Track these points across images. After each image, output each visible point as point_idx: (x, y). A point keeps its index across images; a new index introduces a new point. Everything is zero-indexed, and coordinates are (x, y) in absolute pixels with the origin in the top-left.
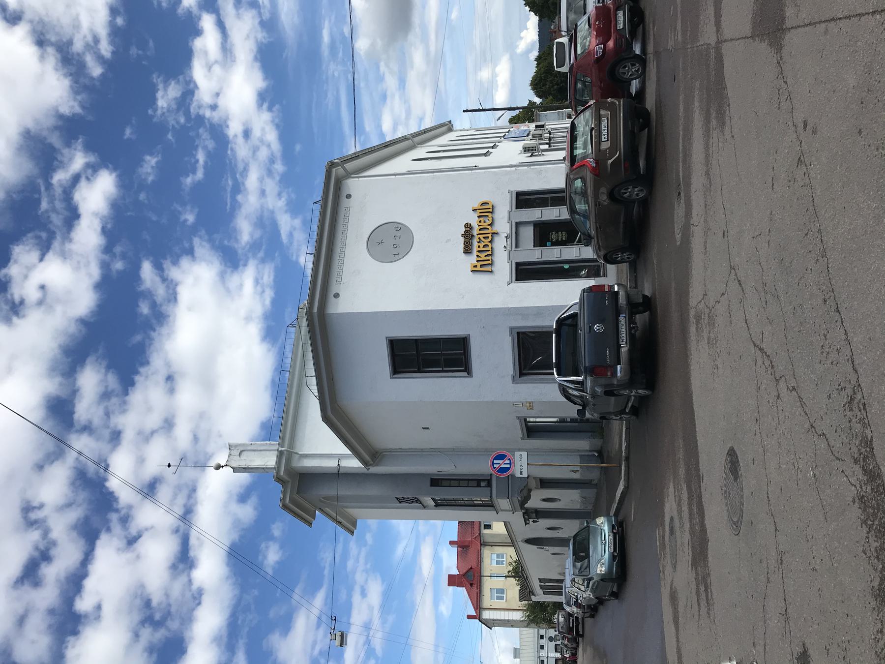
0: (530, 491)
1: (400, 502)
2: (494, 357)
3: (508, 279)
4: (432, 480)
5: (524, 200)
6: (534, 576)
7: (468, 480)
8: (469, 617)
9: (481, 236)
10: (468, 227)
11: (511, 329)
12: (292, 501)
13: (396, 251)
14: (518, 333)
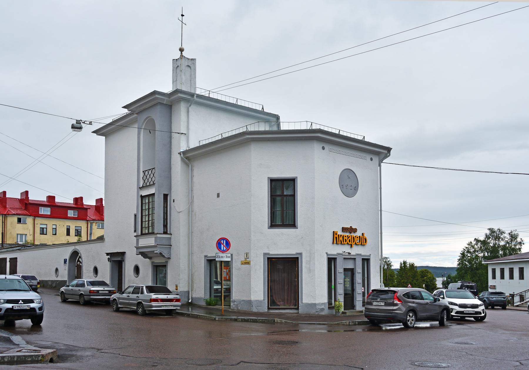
0: (150, 258)
3: (329, 253)
5: (366, 261)
9: (350, 238)
10: (355, 230)
11: (301, 254)
13: (344, 187)
14: (298, 258)
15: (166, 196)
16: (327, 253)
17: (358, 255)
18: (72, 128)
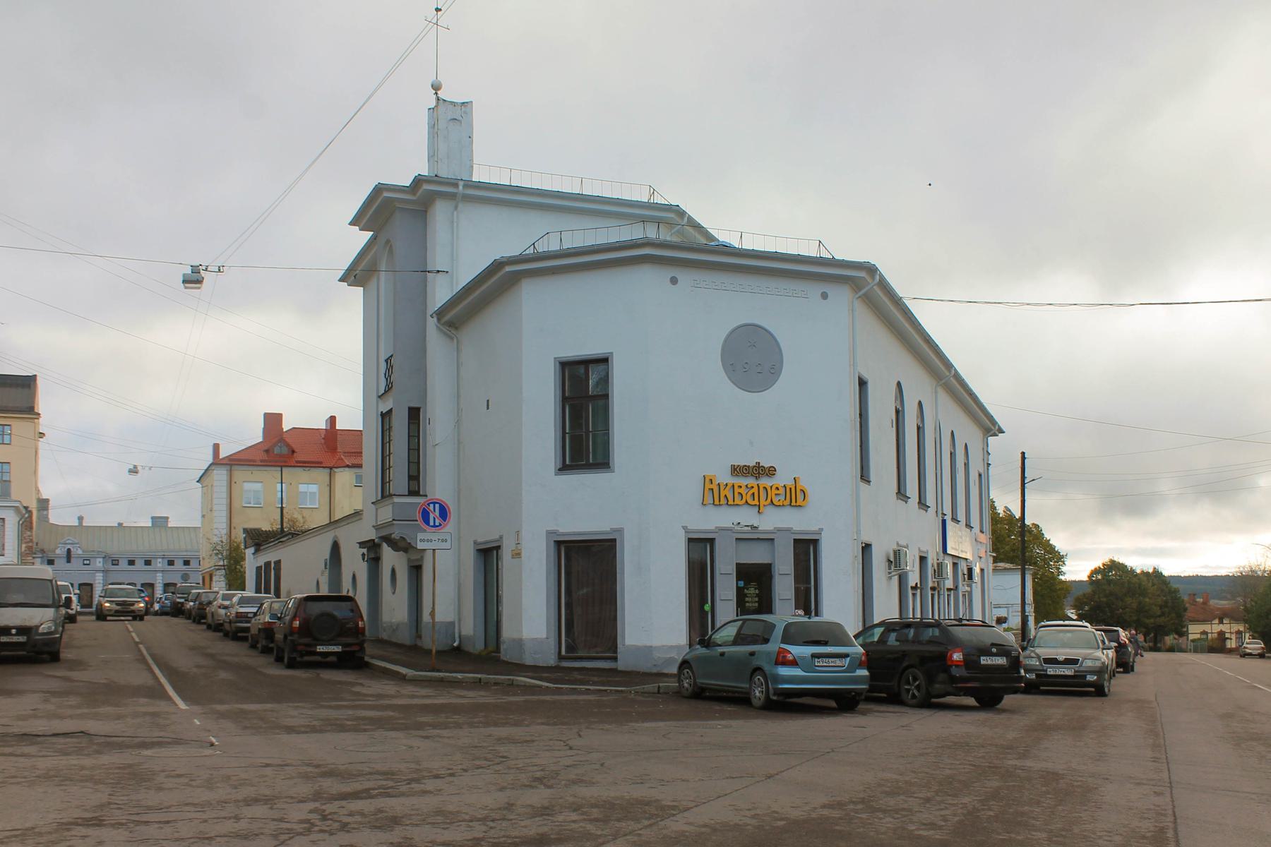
1: (386, 361)
2: (583, 505)
4: (418, 409)
5: (806, 549)
6: (283, 554)
7: (418, 463)
8: (216, 448)
9: (755, 490)
10: (771, 472)
11: (620, 531)
12: (389, 201)
14: (614, 540)
15: (414, 414)
16: (685, 528)
17: (780, 530)
18: (184, 282)
